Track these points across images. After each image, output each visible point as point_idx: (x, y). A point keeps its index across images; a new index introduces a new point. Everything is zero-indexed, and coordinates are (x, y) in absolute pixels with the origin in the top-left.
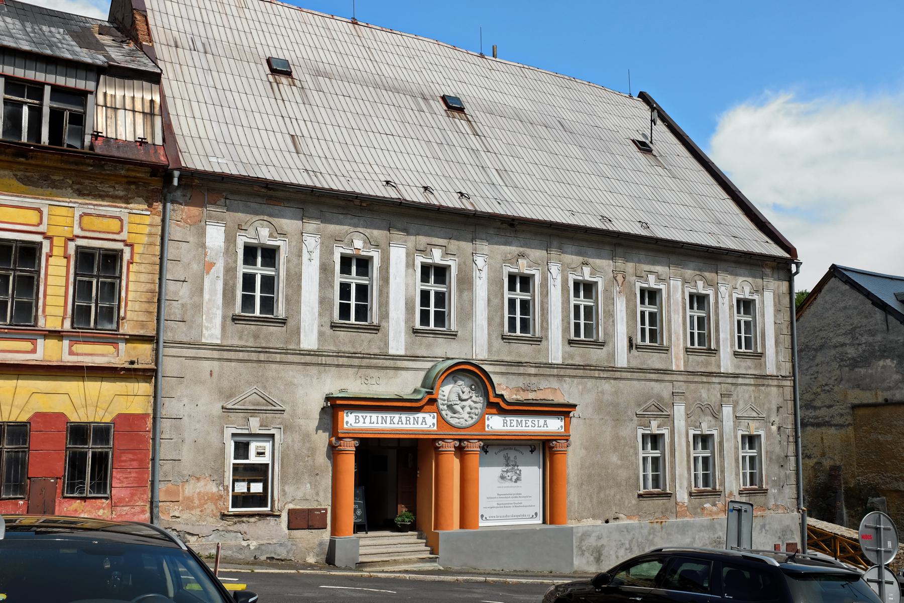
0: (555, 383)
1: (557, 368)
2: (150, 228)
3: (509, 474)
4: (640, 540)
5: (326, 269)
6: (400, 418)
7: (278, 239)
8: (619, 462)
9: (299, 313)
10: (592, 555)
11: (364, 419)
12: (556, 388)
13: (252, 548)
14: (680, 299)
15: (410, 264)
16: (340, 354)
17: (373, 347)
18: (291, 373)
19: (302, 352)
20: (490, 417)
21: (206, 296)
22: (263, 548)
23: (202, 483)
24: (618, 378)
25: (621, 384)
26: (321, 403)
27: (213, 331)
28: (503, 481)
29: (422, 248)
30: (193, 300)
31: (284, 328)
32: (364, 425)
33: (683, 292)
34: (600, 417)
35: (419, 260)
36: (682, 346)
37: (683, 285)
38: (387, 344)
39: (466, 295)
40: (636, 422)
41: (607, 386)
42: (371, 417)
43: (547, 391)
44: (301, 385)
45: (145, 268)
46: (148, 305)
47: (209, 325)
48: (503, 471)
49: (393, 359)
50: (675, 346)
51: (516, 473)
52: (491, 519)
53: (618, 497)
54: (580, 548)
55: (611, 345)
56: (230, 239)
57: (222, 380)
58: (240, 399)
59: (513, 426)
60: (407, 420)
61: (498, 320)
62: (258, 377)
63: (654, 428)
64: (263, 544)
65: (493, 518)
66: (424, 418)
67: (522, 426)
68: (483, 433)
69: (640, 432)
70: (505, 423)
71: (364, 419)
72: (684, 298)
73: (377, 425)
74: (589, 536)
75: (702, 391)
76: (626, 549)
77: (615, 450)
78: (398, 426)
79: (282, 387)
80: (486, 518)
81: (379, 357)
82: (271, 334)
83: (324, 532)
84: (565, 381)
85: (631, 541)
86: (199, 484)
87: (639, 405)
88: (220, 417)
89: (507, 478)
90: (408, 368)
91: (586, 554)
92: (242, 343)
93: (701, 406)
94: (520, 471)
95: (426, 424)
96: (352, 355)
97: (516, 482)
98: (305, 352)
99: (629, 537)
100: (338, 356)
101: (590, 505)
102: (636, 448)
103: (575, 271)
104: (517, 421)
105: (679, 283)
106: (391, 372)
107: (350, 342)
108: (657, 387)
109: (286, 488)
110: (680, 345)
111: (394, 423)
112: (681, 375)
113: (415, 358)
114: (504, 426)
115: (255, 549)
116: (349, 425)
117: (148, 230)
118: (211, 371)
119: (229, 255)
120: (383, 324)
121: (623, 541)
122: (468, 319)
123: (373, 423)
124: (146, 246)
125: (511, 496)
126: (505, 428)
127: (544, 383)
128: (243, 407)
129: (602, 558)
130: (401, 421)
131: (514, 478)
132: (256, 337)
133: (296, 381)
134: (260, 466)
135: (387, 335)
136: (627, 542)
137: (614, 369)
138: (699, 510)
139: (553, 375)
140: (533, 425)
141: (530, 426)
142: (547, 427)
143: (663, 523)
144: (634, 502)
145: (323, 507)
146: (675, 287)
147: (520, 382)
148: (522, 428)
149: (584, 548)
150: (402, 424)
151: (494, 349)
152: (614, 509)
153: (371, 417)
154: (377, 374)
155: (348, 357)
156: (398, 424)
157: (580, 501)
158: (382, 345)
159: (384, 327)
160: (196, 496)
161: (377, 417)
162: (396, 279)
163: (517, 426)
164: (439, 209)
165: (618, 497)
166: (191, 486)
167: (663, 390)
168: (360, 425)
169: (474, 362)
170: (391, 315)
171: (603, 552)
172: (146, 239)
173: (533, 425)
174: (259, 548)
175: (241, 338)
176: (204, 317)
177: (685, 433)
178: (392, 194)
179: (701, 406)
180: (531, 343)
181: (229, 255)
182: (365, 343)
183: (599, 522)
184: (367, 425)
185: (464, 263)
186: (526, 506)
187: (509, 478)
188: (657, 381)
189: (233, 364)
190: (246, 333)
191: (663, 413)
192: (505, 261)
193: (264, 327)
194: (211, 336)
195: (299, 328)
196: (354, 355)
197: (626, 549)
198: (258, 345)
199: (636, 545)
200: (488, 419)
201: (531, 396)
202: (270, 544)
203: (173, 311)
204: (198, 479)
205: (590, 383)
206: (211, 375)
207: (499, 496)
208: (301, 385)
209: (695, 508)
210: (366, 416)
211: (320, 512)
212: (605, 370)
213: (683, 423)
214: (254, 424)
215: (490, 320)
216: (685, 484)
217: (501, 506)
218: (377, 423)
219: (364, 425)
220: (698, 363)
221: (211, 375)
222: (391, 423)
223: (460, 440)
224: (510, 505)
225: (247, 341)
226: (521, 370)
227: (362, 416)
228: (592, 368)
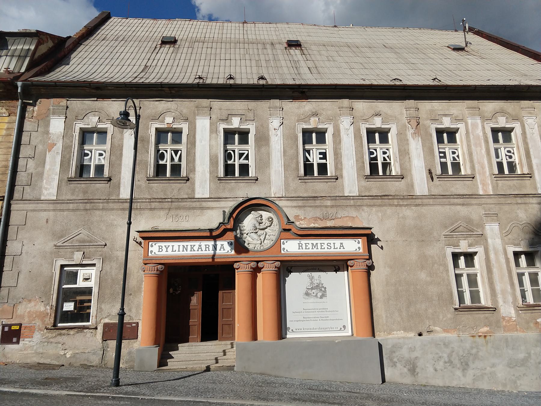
0: (353, 213)
1: (353, 199)
2: (8, 125)
3: (314, 291)
4: (461, 353)
5: (143, 140)
6: (200, 246)
7: (106, 123)
8: (428, 279)
9: (120, 173)
10: (404, 367)
11: (167, 249)
12: (355, 216)
13: (68, 356)
14: (481, 134)
15: (213, 130)
16: (152, 200)
17: (182, 193)
18: (112, 217)
19: (120, 201)
20: (285, 242)
21: (47, 167)
22: (78, 356)
23: (33, 304)
24: (419, 205)
25: (424, 210)
26: (327, 295)
27: (51, 191)
28: (307, 297)
29: (224, 118)
30: (37, 170)
31: (108, 185)
32: (167, 253)
33: (483, 128)
34: (404, 239)
35: (222, 126)
36: (488, 173)
37: (483, 122)
38: (193, 191)
39: (263, 149)
40: (443, 242)
41: (409, 213)
42: (173, 246)
43: (345, 219)
44: (120, 226)
45: (1, 151)
46: (2, 176)
47: (48, 187)
48: (308, 289)
49: (198, 201)
50: (480, 174)
51: (321, 290)
52: (298, 331)
53: (430, 311)
54: (391, 360)
55: (409, 178)
56: (68, 127)
57: (55, 225)
58: (69, 239)
59: (309, 249)
60: (206, 248)
61: (293, 165)
62: (84, 222)
63: (464, 247)
64: (78, 353)
65: (300, 331)
66: (222, 245)
67: (317, 249)
68: (280, 255)
69: (449, 251)
70: (300, 246)
71: (167, 249)
72: (485, 133)
73: (179, 253)
74: (401, 348)
75: (518, 211)
76: (445, 362)
77: (422, 268)
78: (198, 252)
79: (104, 228)
80: (292, 330)
81: (186, 200)
82: (98, 189)
83: (135, 342)
84: (363, 210)
85: (450, 356)
86: (29, 305)
87: (446, 227)
88: (51, 253)
89: (312, 294)
90: (213, 208)
91: (398, 365)
92: (74, 198)
93: (519, 225)
94: (325, 288)
95: (224, 250)
96: (162, 200)
97: (321, 298)
98: (123, 201)
99: (448, 351)
100: (151, 202)
101: (399, 319)
102: (446, 266)
103: (367, 122)
104: (312, 244)
105: (479, 121)
106: (198, 212)
107: (162, 191)
108: (463, 211)
109: (103, 306)
110: (486, 172)
111: (194, 251)
112: (491, 198)
113: (219, 199)
114: (299, 249)
115: (70, 357)
116: (153, 253)
117: (6, 126)
118: (47, 219)
119: (68, 137)
120: (191, 176)
121: (440, 355)
122: (267, 167)
123: (175, 251)
124: (4, 137)
125: (317, 310)
126: (301, 250)
127: (341, 213)
128: (70, 245)
129: (418, 370)
130: (201, 248)
131: (320, 294)
132: (85, 192)
133: (115, 222)
134: (76, 289)
135: (193, 184)
136: (445, 355)
137: (412, 197)
138: (532, 325)
139: (351, 206)
140: (329, 247)
141: (326, 248)
142: (344, 248)
143: (488, 338)
144: (449, 316)
145: (134, 321)
146: (475, 126)
147: (318, 213)
148: (317, 250)
149: (395, 360)
150: (202, 250)
151: (292, 188)
152: (428, 323)
153: (173, 246)
154: (185, 214)
155: (160, 202)
156: (198, 251)
157: (388, 315)
158: (190, 191)
159: (192, 178)
160: (26, 314)
161: (179, 246)
162: (201, 142)
163: (312, 249)
164: (475, 90)
165: (430, 311)
166: (23, 307)
167: (471, 213)
168: (164, 253)
169: (270, 199)
170: (197, 169)
171: (418, 364)
172: (5, 132)
173: (329, 247)
174: (74, 356)
175: (73, 194)
176: (45, 181)
177: (502, 250)
178: (436, 83)
179: (519, 225)
180: (326, 180)
181: (68, 137)
182: (175, 191)
183: (412, 335)
184: (170, 253)
185: (262, 125)
186: (333, 320)
187: (314, 294)
188: (463, 205)
189: (65, 213)
190: (77, 190)
191: (474, 233)
192: (298, 121)
193: (92, 185)
194: (49, 194)
195: (119, 184)
196: (164, 200)
197: (445, 362)
198: (86, 198)
199: (457, 358)
200: (284, 244)
201: (329, 224)
202: (85, 353)
203: (20, 178)
204: (30, 301)
205: (389, 211)
206: (47, 222)
207: (304, 311)
208: (120, 226)
209: (528, 323)
210: (169, 246)
211: (131, 325)
212: (403, 198)
213: (498, 241)
214: (77, 257)
215: (286, 167)
216: (510, 299)
217: (307, 319)
218: (179, 251)
219: (167, 253)
220: (510, 187)
221: (47, 222)
222: (191, 251)
223: (258, 262)
224: (316, 319)
225: (77, 196)
226: (318, 203)
227: (165, 246)
228: (390, 197)
